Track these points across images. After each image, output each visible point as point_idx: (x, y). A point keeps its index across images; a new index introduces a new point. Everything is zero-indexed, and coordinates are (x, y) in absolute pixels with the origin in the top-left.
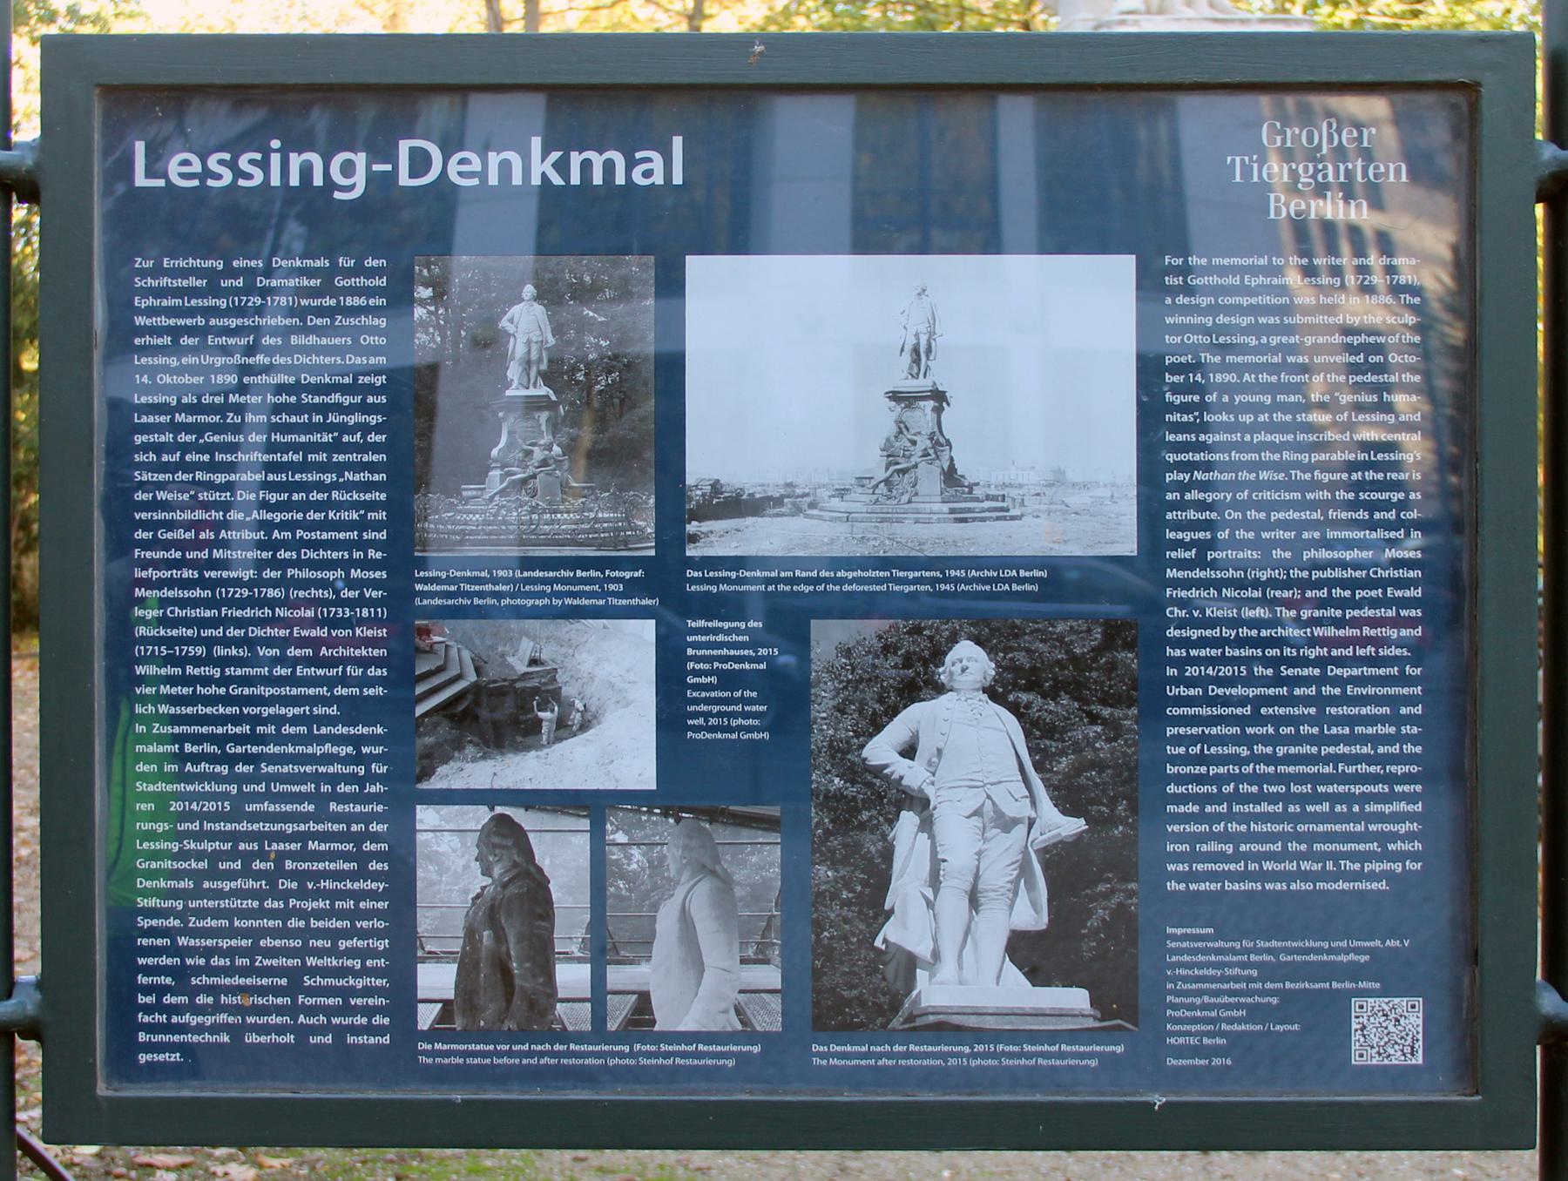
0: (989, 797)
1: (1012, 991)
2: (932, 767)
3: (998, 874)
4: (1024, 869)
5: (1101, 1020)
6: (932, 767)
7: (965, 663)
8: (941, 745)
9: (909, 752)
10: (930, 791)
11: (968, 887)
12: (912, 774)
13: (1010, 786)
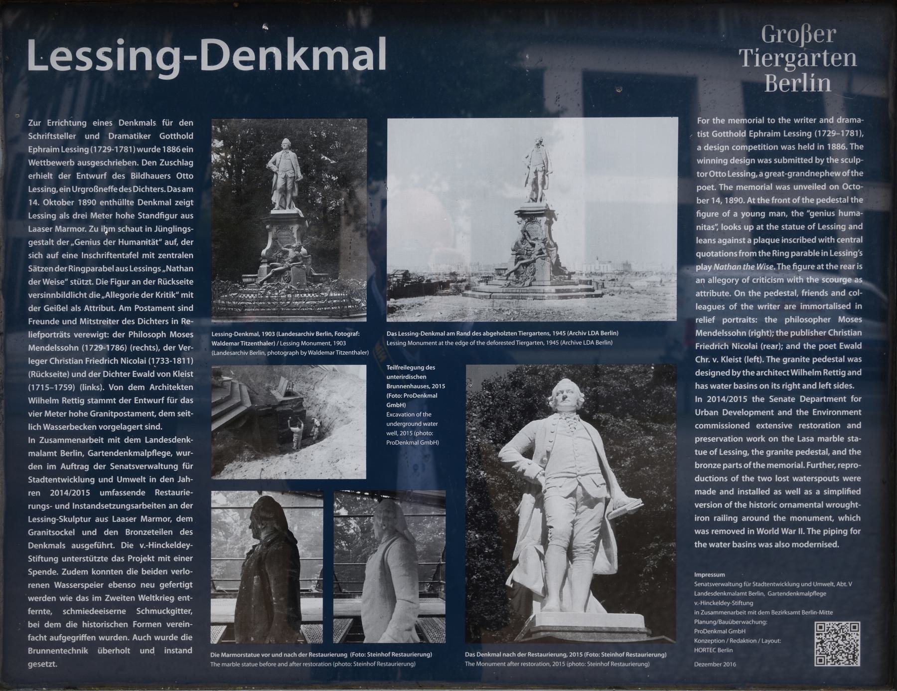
0: (580, 484)
1: (595, 616)
2: (544, 464)
3: (586, 537)
4: (602, 533)
5: (652, 636)
6: (544, 464)
7: (565, 393)
8: (549, 449)
9: (528, 453)
10: (542, 480)
11: (566, 545)
12: (530, 468)
13: (593, 476)
